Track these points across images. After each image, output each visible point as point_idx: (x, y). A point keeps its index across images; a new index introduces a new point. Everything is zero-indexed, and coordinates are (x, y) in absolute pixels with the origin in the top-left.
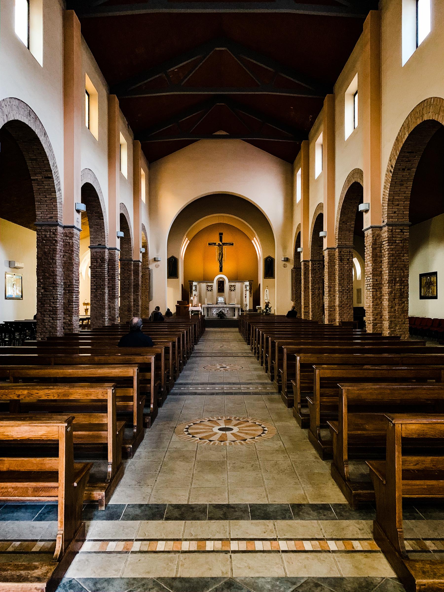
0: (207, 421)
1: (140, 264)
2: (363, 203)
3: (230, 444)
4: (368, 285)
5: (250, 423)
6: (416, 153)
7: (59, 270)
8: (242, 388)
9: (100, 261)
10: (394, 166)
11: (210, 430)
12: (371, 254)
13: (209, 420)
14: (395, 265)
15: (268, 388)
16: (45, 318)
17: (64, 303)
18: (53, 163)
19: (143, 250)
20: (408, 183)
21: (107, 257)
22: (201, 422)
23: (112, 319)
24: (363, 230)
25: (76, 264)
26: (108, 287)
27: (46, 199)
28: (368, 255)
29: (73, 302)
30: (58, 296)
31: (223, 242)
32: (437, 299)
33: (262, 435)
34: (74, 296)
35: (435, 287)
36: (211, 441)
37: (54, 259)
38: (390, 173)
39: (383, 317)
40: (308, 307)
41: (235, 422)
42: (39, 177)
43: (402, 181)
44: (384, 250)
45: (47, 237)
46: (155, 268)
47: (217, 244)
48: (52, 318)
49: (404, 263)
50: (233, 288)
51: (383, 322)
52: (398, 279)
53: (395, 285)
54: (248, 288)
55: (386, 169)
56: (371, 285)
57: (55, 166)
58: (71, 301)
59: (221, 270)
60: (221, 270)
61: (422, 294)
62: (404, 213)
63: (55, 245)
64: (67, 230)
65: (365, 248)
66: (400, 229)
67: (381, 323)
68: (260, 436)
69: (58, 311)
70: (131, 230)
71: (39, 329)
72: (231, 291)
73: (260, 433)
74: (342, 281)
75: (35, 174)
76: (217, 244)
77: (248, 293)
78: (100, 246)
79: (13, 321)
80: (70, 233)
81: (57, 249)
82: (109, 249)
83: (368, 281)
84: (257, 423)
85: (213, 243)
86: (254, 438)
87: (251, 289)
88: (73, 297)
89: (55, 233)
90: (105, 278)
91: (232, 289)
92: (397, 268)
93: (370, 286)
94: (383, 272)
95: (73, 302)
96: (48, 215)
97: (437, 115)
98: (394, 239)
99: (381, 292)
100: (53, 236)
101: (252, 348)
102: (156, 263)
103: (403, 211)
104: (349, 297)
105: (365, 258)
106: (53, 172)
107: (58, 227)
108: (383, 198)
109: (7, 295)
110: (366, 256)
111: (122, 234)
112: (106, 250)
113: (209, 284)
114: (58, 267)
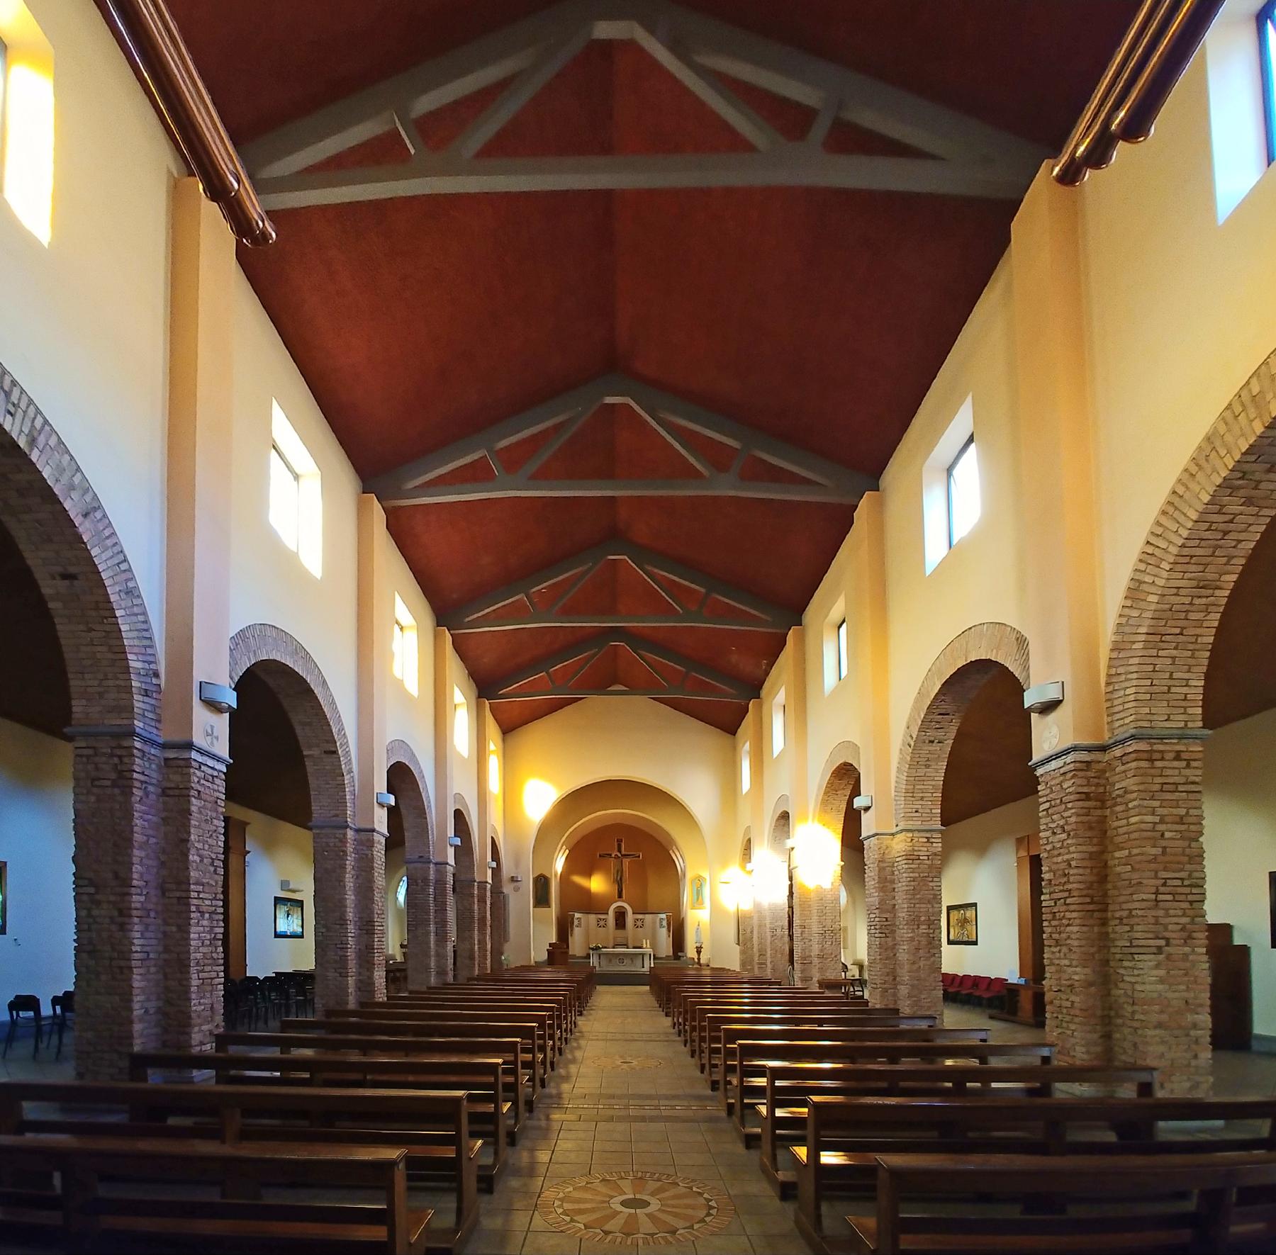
0: (598, 1181)
1: (489, 886)
2: (860, 795)
3: (646, 1242)
4: (873, 927)
5: (681, 1189)
6: (953, 715)
7: (350, 898)
8: (662, 1108)
9: (422, 882)
10: (914, 736)
11: (604, 1205)
12: (876, 878)
13: (603, 1180)
14: (918, 896)
15: (708, 1108)
16: (328, 974)
17: (360, 949)
18: (337, 729)
19: (494, 864)
20: (939, 764)
21: (432, 876)
22: (587, 1183)
23: (441, 972)
24: (1029, 764)
25: (379, 889)
26: (436, 923)
27: (327, 786)
28: (871, 879)
29: (374, 949)
30: (350, 939)
31: (623, 853)
32: (977, 945)
33: (708, 1219)
34: (376, 940)
35: (975, 927)
36: (607, 1233)
37: (342, 881)
38: (908, 747)
39: (897, 979)
40: (764, 955)
41: (652, 1185)
42: (315, 752)
43: (928, 760)
44: (899, 870)
45: (329, 846)
46: (513, 891)
47: (613, 856)
48: (340, 973)
49: (932, 892)
50: (639, 923)
51: (898, 987)
52: (923, 918)
53: (918, 928)
54: (665, 923)
55: (900, 742)
56: (877, 927)
57: (342, 733)
58: (371, 947)
59: (620, 896)
60: (620, 896)
61: (952, 937)
62: (933, 811)
63: (343, 859)
64: (363, 836)
65: (866, 867)
66: (927, 838)
67: (895, 988)
68: (702, 1221)
69: (349, 962)
70: (474, 834)
71: (318, 988)
72: (637, 927)
73: (702, 1213)
74: (824, 917)
75: (310, 748)
76: (613, 856)
77: (664, 930)
78: (421, 860)
79: (290, 971)
80: (368, 840)
81: (346, 864)
82: (436, 864)
83: (872, 920)
84: (694, 1189)
85: (608, 855)
86: (692, 1227)
87: (669, 925)
88: (374, 941)
89: (343, 841)
90: (430, 906)
91: (638, 925)
92: (921, 901)
93: (876, 929)
94: (897, 907)
95: (374, 949)
96: (331, 812)
97: (995, 651)
98: (915, 853)
99: (894, 939)
100: (340, 844)
101: (675, 1024)
102: (516, 884)
103: (931, 809)
104: (834, 943)
105: (866, 884)
106: (338, 744)
107: (348, 829)
108: (896, 787)
109: (278, 930)
110: (866, 880)
111: (458, 841)
112: (432, 866)
113: (602, 917)
114: (349, 893)
